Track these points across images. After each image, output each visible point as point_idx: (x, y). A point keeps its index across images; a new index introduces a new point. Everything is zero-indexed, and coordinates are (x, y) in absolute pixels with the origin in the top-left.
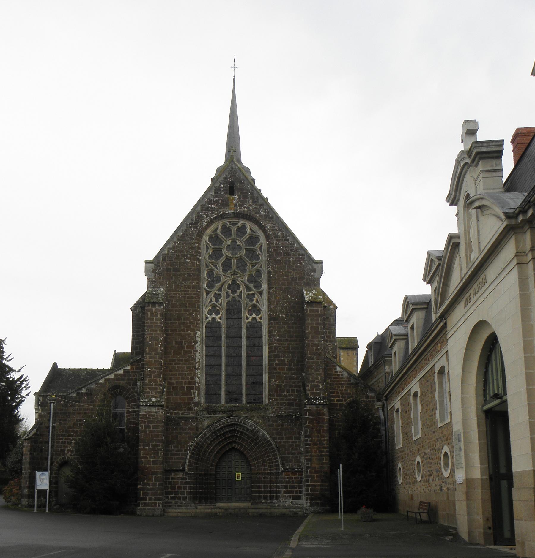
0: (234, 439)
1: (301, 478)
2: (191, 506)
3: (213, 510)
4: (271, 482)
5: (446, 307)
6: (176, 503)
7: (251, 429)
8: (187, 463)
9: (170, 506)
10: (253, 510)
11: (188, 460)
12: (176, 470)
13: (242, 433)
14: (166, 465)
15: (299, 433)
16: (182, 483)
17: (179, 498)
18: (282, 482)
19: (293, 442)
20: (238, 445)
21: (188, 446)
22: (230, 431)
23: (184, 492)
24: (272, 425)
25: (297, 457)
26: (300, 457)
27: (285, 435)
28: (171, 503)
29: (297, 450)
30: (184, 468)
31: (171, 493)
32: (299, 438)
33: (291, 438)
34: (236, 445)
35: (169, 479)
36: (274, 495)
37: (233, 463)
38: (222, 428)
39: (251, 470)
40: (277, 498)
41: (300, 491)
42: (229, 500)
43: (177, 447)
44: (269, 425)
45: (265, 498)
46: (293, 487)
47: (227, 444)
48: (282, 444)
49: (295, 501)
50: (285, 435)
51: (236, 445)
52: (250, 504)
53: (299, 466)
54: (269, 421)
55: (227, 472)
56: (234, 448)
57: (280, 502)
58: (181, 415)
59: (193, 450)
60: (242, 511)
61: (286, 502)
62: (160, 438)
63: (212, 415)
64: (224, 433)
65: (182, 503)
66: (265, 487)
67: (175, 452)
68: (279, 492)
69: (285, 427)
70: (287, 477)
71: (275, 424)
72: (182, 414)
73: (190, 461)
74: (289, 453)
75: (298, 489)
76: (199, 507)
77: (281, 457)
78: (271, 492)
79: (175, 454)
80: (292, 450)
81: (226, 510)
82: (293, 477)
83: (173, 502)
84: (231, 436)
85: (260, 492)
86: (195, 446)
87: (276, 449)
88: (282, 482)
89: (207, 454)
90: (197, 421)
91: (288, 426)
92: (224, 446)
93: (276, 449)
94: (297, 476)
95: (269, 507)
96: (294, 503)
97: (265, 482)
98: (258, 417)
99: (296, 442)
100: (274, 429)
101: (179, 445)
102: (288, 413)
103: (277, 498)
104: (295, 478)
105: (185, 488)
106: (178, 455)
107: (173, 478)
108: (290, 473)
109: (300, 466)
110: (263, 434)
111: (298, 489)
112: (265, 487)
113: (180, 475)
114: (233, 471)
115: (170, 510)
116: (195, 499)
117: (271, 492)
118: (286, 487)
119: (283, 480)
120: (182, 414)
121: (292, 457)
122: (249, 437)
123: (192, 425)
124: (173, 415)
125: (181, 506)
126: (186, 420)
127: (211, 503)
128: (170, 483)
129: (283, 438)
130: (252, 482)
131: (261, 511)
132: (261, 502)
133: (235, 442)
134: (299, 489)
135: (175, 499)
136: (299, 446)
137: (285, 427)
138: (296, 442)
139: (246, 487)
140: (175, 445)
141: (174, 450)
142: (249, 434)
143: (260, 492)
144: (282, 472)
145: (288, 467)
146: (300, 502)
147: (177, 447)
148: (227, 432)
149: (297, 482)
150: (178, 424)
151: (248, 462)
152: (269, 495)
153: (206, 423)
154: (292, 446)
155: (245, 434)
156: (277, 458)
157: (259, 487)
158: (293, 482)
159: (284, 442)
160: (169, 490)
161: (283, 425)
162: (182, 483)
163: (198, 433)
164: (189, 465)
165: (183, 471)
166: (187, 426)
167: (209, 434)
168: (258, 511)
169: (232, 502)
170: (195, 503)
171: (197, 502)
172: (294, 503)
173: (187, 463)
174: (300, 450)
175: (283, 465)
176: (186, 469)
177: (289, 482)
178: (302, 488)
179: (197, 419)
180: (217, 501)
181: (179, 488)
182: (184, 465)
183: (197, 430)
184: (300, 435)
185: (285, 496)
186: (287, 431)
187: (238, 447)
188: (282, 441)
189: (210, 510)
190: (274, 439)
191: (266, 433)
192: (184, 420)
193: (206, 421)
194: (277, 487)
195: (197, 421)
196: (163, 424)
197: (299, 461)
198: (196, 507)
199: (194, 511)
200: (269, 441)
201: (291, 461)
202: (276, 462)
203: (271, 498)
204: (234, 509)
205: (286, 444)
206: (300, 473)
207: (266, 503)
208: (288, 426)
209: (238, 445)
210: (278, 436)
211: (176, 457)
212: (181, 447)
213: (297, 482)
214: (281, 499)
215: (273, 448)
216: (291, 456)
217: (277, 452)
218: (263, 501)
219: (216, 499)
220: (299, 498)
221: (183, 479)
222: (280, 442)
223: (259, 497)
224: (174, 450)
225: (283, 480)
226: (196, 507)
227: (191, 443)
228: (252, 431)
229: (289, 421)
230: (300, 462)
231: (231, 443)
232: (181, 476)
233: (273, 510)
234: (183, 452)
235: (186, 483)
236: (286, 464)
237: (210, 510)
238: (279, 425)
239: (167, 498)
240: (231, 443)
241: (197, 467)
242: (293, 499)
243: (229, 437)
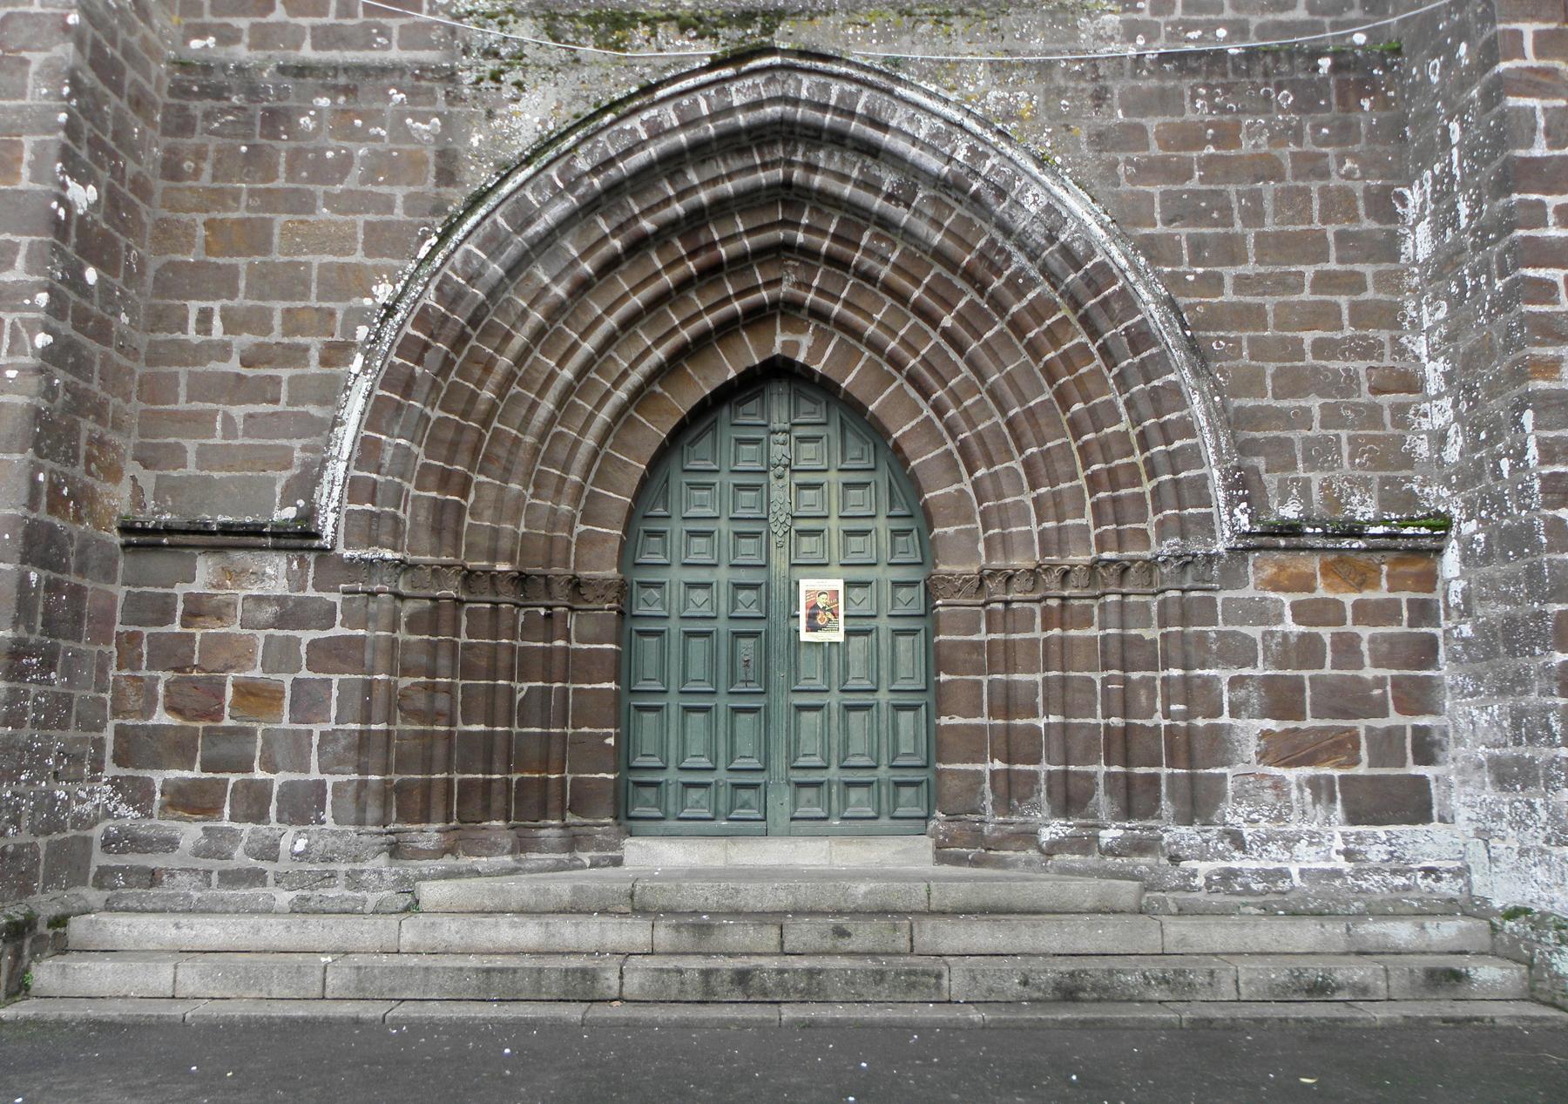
0: (785, 289)
1: (1423, 612)
2: (354, 880)
3: (568, 932)
4: (1125, 653)
5: (486, 1021)
6: (215, 847)
7: (934, 165)
8: (338, 470)
9: (153, 878)
10: (983, 936)
11: (347, 436)
12: (226, 529)
13: (857, 216)
14: (148, 479)
15: (1384, 205)
16: (281, 656)
17: (254, 804)
18: (1238, 652)
19: (1325, 282)
20: (821, 339)
21: (361, 316)
22: (749, 201)
23: (299, 743)
24: (1133, 136)
25: (1372, 416)
26: (1401, 421)
27: (1254, 215)
28: (170, 844)
29: (1368, 350)
30: (309, 515)
31: (179, 749)
32: (1389, 248)
33: (1313, 248)
34: (806, 340)
35: (165, 616)
36: (1158, 772)
37: (780, 492)
38: (673, 163)
39: (929, 551)
40: (1198, 803)
41: (1421, 733)
42: (739, 806)
43: (260, 322)
44: (1100, 139)
45: (1070, 799)
46: (1349, 700)
47: (727, 329)
48: (1229, 296)
49: (1378, 840)
50: (1254, 215)
51: (806, 340)
52: (925, 845)
53: (1398, 499)
54: (1100, 97)
55: (723, 575)
56: (780, 371)
57: (1238, 841)
58: (307, 53)
59: (408, 347)
60: (865, 935)
61: (1290, 842)
62: (25, 183)
63: (588, 50)
64: (698, 217)
65: (269, 851)
66: (1063, 696)
67: (234, 366)
68: (1219, 745)
69: (1247, 146)
70: (1287, 599)
71: (1152, 123)
72: (325, 38)
73: (367, 452)
74: (1293, 384)
75: (1394, 719)
76: (431, 892)
77: (1234, 421)
78: (1123, 745)
79: (237, 389)
80: (1320, 348)
81: (699, 924)
82: (1349, 599)
83: (191, 832)
84: (761, 253)
85: (1014, 746)
86: (423, 318)
87: (1170, 338)
88: (1238, 652)
89: (547, 405)
90: (453, 99)
91: (1277, 139)
92: (702, 342)
93: (1170, 338)
94: (1382, 593)
95: (1127, 891)
96: (1376, 853)
97: (1061, 653)
98: (997, 68)
99: (1355, 283)
100: (1147, 171)
101: (279, 306)
102: (1263, 31)
103: (1198, 803)
104: (1364, 612)
105: (308, 702)
106: (265, 390)
107: (197, 610)
108: (1314, 564)
109: (1412, 499)
110: (1053, 214)
111: (1394, 719)
112: (1063, 696)
113: (274, 574)
114: (779, 562)
115: (122, 928)
116: (410, 803)
117: (1123, 745)
118: (1282, 699)
119: (1255, 632)
120: (325, 38)
121: (1332, 417)
122: (921, 254)
123: (403, 134)
124: (242, 52)
125: (257, 877)
126: (349, 91)
127: (573, 842)
128: (172, 654)
129: (1231, 251)
130: (936, 659)
131: (1051, 936)
132: (1028, 837)
133: (789, 310)
134: (1409, 722)
135: (212, 810)
136: (1389, 316)
137: (1247, 146)
138: (1355, 283)
139: (883, 697)
140: (241, 301)
141: (224, 351)
142: (922, 228)
143: (1014, 746)
144: (1238, 553)
145: (1291, 512)
146: (1427, 843)
147: (260, 322)
148: (722, 208)
149: (1388, 653)
150: (277, 120)
151: (907, 483)
152: (1101, 769)
153: (532, 113)
154: (1324, 316)
155: (884, 223)
156: (1188, 429)
157: (1008, 702)
158: (1347, 649)
159: (1242, 284)
160: (161, 718)
161: (1227, 136)
162: (281, 656)
163: (456, 199)
164: (354, 489)
165: (299, 537)
166: (361, 136)
167: (559, 209)
168: (1024, 936)
169: (762, 828)
170: (396, 851)
171: (429, 835)
172: (1376, 853)
173: (338, 470)
174: (1401, 351)
175: (1244, 485)
176: (328, 523)
177: (1308, 650)
178: (1432, 709)
179: (451, 76)
180: (626, 821)
181: (256, 697)
182: (307, 483)
183: (447, 175)
184: (1394, 217)
185: (1278, 785)
186: (1269, 188)
187: (815, 352)
188: (1229, 272)
189: (530, 933)
190: (1153, 249)
191: (1076, 204)
192: (334, 91)
193: (532, 98)
194: (1199, 696)
195: (453, 99)
196: (65, 51)
197: (1393, 456)
198: (406, 885)
199: (366, 932)
200: (1105, 273)
201: (1320, 453)
202: (1175, 461)
203: (1134, 799)
204: (776, 917)
205: (1269, 302)
206: (1416, 552)
207: (1084, 844)
208: (1277, 139)
209: (821, 339)
210: (1182, 232)
211: (238, 411)
212: (293, 322)
213: (1388, 653)
214: (1234, 814)
215: (1141, 338)
216: (1314, 403)
217: (1182, 374)
218: (1053, 829)
219: (627, 803)
220: (1413, 804)
221: (291, 614)
222: (1213, 283)
223: (1011, 791)
224: (224, 351)
225: (1255, 632)
226: (406, 885)
227: (383, 292)
228: (951, 187)
229: (1286, 98)
230: (1408, 461)
231: (758, 317)
232: (280, 588)
233: (1177, 931)
234: (314, 368)
235: (324, 654)
236: (1271, 480)
237: (530, 933)
238: (1191, 137)
239: (138, 794)
240: (758, 317)
241: (439, 507)
242: (1353, 818)
243: (741, 262)
